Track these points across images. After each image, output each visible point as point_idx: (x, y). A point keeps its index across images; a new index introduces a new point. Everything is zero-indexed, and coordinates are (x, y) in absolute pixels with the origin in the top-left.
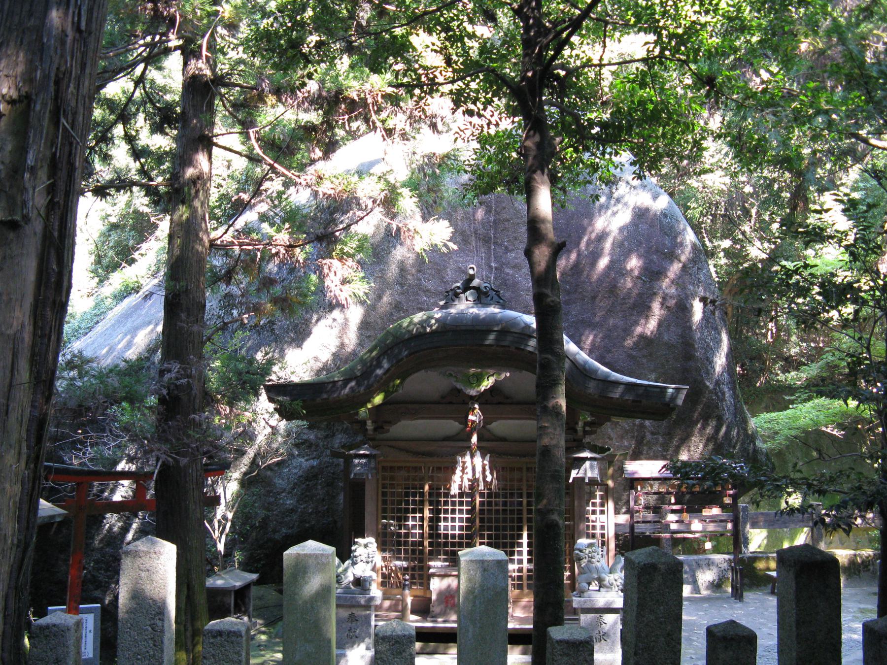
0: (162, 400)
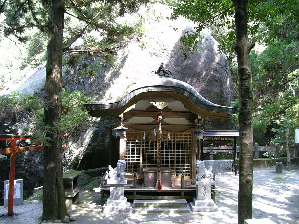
0: (46, 112)
